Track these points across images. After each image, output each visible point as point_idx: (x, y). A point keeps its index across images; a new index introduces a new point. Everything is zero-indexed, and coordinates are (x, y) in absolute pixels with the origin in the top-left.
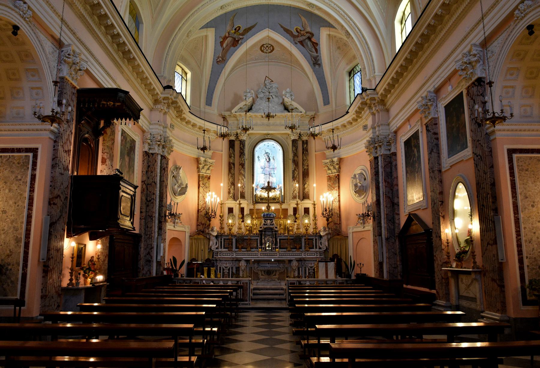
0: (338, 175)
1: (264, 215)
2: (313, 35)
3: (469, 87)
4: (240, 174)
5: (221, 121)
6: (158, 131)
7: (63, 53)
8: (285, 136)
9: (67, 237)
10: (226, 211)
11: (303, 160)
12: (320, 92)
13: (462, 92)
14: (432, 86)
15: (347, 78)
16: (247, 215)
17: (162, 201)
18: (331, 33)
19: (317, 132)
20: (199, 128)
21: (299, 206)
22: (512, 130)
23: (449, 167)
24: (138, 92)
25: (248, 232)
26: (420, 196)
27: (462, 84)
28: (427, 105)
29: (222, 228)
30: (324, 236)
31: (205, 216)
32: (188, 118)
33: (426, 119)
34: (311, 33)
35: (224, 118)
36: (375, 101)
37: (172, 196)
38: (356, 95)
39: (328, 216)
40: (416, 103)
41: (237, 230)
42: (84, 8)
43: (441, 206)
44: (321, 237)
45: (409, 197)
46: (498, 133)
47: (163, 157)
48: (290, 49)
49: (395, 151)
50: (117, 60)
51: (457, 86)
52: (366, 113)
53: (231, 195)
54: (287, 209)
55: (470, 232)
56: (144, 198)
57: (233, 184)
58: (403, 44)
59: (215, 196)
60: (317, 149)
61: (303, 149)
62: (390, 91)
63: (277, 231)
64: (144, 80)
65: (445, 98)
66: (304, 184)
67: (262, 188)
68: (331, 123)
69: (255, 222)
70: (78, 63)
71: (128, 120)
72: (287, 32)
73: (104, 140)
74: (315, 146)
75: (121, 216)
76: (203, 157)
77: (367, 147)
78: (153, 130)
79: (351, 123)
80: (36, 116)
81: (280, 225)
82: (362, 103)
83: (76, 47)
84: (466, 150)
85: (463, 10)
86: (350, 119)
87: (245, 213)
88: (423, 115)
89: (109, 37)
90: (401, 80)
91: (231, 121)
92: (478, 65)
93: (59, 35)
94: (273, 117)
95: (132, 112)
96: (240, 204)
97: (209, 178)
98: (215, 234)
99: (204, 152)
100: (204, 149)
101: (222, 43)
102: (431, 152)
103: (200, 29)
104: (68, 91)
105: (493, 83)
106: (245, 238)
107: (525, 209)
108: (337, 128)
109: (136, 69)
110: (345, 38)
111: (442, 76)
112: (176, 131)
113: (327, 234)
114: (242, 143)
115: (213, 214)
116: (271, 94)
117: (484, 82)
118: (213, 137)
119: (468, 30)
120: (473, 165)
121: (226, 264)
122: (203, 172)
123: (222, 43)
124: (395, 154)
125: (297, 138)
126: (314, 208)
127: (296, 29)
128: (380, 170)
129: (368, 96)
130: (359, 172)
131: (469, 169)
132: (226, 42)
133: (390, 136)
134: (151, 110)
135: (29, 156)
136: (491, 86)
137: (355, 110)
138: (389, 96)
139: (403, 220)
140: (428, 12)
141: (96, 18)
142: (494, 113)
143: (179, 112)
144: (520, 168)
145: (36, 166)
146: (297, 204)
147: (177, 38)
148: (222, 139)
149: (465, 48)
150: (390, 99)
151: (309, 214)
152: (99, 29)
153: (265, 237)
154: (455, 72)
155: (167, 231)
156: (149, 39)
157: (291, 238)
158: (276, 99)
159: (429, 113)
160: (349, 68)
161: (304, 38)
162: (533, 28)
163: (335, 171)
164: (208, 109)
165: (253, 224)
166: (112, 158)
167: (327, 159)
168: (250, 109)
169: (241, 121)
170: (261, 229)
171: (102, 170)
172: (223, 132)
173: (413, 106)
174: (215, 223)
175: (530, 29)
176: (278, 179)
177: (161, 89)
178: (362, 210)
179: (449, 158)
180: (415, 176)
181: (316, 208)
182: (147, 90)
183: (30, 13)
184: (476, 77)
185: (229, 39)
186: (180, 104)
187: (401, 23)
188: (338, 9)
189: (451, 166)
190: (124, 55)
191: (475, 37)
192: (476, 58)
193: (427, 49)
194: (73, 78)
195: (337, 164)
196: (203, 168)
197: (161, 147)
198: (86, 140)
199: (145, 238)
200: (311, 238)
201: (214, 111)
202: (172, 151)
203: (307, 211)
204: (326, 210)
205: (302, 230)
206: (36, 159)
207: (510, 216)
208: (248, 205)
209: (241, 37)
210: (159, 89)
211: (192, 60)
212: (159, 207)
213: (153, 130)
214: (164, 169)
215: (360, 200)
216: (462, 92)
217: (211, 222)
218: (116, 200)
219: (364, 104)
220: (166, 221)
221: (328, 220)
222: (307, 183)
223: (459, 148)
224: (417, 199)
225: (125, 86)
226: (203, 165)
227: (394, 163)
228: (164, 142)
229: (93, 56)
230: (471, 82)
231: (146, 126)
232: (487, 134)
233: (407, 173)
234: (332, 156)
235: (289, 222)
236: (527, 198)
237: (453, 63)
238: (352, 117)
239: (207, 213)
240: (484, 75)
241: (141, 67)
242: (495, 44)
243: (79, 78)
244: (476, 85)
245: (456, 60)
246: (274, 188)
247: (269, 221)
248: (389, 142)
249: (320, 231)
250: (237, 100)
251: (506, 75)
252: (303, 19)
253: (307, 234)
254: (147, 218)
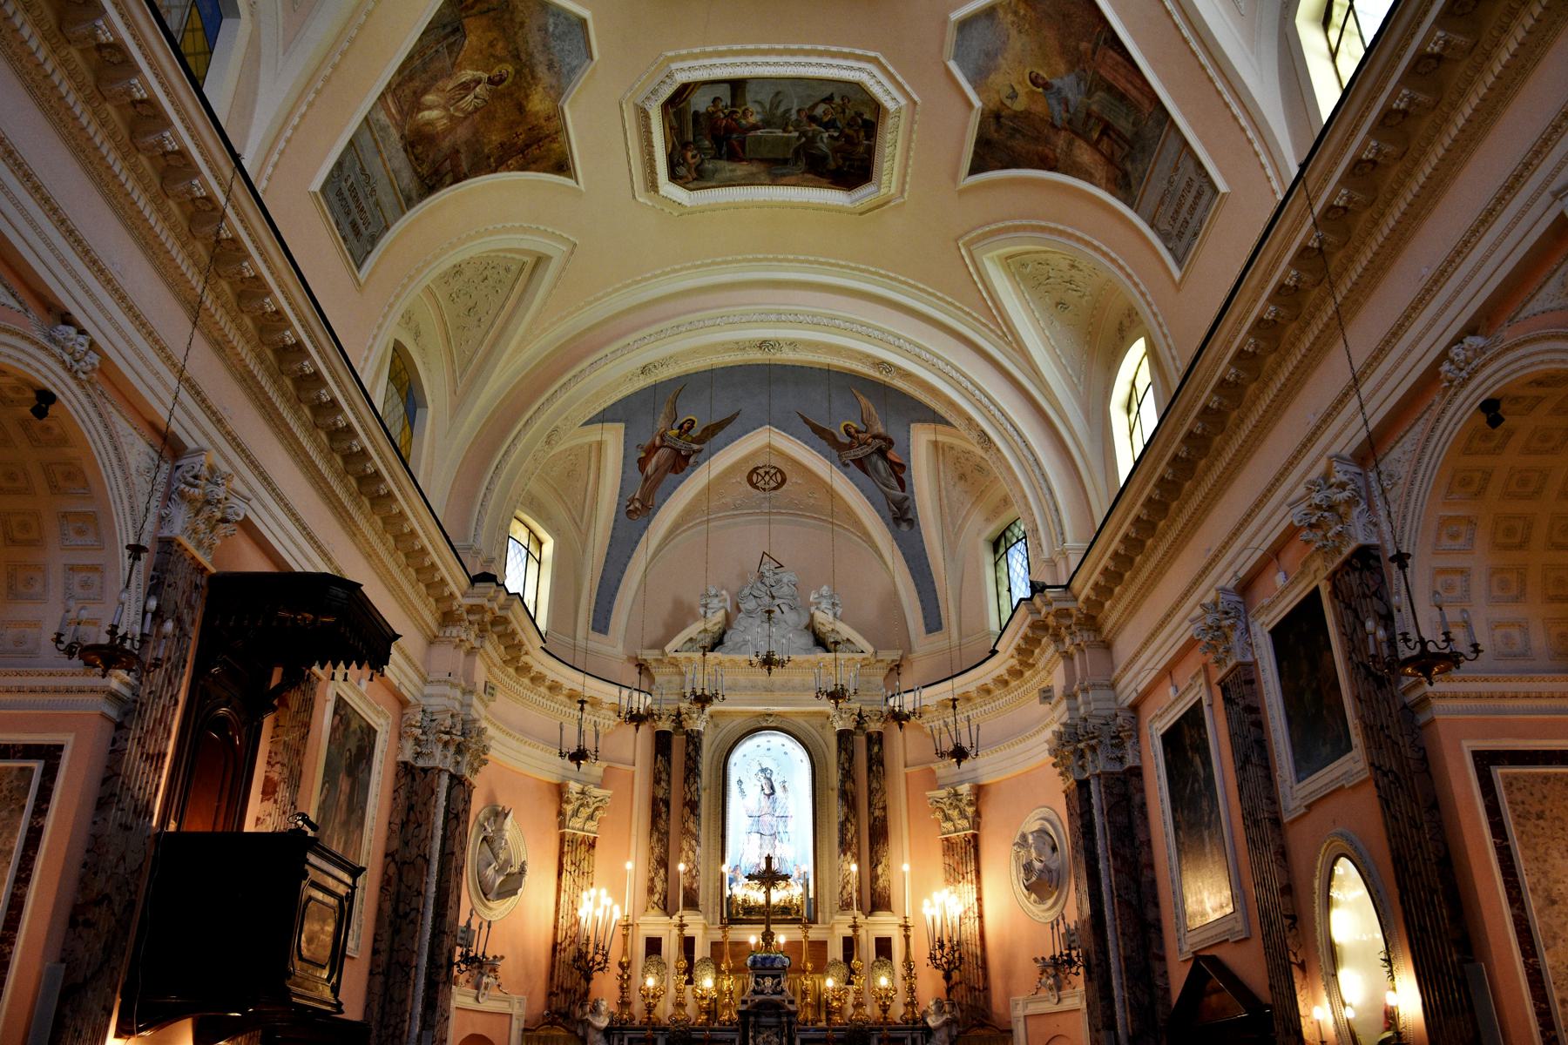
0: (975, 836)
1: (754, 962)
2: (890, 443)
3: (1335, 573)
4: (686, 832)
5: (632, 675)
6: (446, 702)
7: (178, 474)
8: (817, 721)
9: (117, 1036)
10: (641, 947)
11: (871, 792)
12: (915, 594)
13: (1317, 589)
14: (1229, 574)
15: (989, 558)
16: (704, 960)
17: (445, 916)
18: (940, 438)
19: (908, 708)
20: (570, 697)
21: (861, 932)
22: (1479, 696)
23: (1303, 810)
24: (394, 589)
25: (704, 1017)
26: (1224, 901)
27: (1314, 567)
28: (1219, 628)
29: (624, 1004)
30: (937, 1029)
31: (573, 964)
32: (537, 668)
33: (1220, 667)
34: (885, 439)
35: (642, 667)
36: (1070, 621)
37: (475, 900)
38: (1015, 603)
39: (948, 962)
40: (1546, 197)
41: (670, 1009)
42: (258, 356)
43: (1288, 930)
44: (929, 1032)
45: (1191, 905)
46: (1438, 704)
47: (457, 781)
48: (828, 479)
49: (1137, 763)
50: (339, 500)
51: (1302, 573)
52: (1047, 652)
53: (656, 897)
54: (825, 943)
55: (1390, 1017)
56: (388, 906)
57: (663, 863)
58: (1137, 463)
59: (606, 900)
60: (909, 757)
61: (870, 759)
62: (1112, 591)
63: (795, 1014)
64: (415, 558)
65: (1273, 604)
66: (874, 864)
67: (750, 877)
68: (949, 683)
69: (727, 984)
70: (219, 501)
71: (354, 665)
72: (821, 435)
73: (276, 726)
74: (904, 748)
75: (298, 964)
76: (577, 781)
77: (1054, 752)
78: (433, 701)
79: (1006, 683)
80: (62, 647)
81: (804, 993)
82: (1033, 626)
83: (219, 455)
84: (1348, 756)
85: (1296, 368)
86: (1002, 671)
87: (697, 956)
88: (1211, 658)
89: (323, 436)
90: (1188, 485)
91: (662, 676)
92: (1355, 512)
93: (165, 415)
94: (781, 663)
95: (368, 642)
96: (682, 926)
97: (592, 846)
98: (603, 1022)
99: (579, 765)
100: (579, 756)
101: (642, 463)
102: (1242, 764)
103: (586, 424)
104: (181, 577)
105: (1409, 556)
106: (695, 1035)
107: (1554, 938)
108: (968, 698)
109: (394, 525)
110: (978, 451)
111: (1254, 544)
112: (501, 704)
113: (947, 1024)
114: (694, 740)
115: (599, 958)
116: (777, 601)
117: (1377, 559)
118: (607, 720)
119: (1314, 420)
120: (1376, 801)
122: (576, 826)
123: (642, 463)
124: (1137, 772)
125: (851, 726)
126: (907, 938)
127: (846, 428)
128: (1098, 819)
129: (1049, 604)
130: (1036, 826)
131: (1366, 811)
132: (654, 460)
133: (1120, 720)
134: (432, 641)
135: (31, 770)
136: (1403, 566)
137: (1013, 645)
138: (1108, 604)
139: (1178, 976)
140: (1199, 376)
141: (288, 382)
142: (1422, 642)
143: (513, 648)
144: (1520, 808)
145: (48, 801)
146: (855, 927)
147: (520, 446)
148: (632, 727)
149: (1313, 465)
150: (1112, 614)
151: (890, 957)
152: (296, 412)
153: (757, 1033)
154: (1291, 533)
155: (453, 1014)
156: (440, 449)
157: (836, 1035)
158: (791, 617)
159: (1227, 651)
160: (992, 529)
161: (868, 450)
162: (1498, 407)
163: (965, 823)
164: (597, 642)
165: (720, 992)
166: (295, 780)
167: (940, 787)
168: (717, 643)
169: (689, 676)
170: (744, 1008)
171: (260, 816)
172: (635, 707)
173: (1180, 631)
174: (605, 988)
175: (1491, 409)
176: (796, 850)
177: (464, 581)
178: (1051, 947)
179: (1299, 781)
180: (1203, 841)
181: (912, 940)
182: (422, 586)
183: (94, 359)
184: (1353, 545)
185: (663, 453)
186: (515, 625)
187: (1129, 411)
188: (954, 373)
189: (1309, 807)
190: (361, 484)
191: (1337, 436)
192: (1347, 494)
193: (1205, 474)
194: (199, 544)
195: (970, 803)
196: (576, 813)
197: (452, 749)
198: (221, 724)
199: (379, 1036)
200: (898, 1034)
201: (614, 647)
202: (485, 762)
203: (884, 946)
204: (942, 946)
205: (871, 1011)
206: (53, 779)
207: (1513, 964)
208: (706, 928)
209: (696, 447)
210: (456, 581)
211: (559, 504)
212: (433, 936)
213: (433, 701)
214: (457, 817)
215: (1042, 913)
216: (1317, 589)
217: (593, 985)
218: (290, 913)
219: (1039, 626)
220: (450, 981)
221: (947, 977)
223: (1326, 750)
224: (1214, 910)
225: (354, 568)
226: (577, 804)
227: (1137, 799)
228: (463, 734)
229: (269, 484)
230: (1338, 560)
231: (412, 689)
232: (1405, 706)
233: (1177, 828)
234: (956, 779)
235: (830, 983)
236: (1553, 902)
237: (1285, 508)
238: (1006, 666)
239: (581, 956)
240: (1374, 540)
241: (407, 519)
242: (1396, 453)
243: (218, 542)
244: (1355, 569)
245: (1291, 499)
246: (786, 877)
247: (768, 982)
248: (1118, 737)
249: (925, 1014)
250: (679, 617)
251: (1438, 538)
252: (864, 401)
253: (885, 1023)
254: (390, 967)
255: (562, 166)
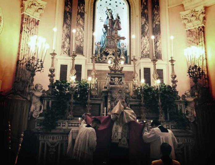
0: (203, 27)
53: (66, 49)
97: (37, 23)
121: (53, 138)
222: (160, 41)
239: (28, 65)
247: (117, 79)
255: (50, 54)
